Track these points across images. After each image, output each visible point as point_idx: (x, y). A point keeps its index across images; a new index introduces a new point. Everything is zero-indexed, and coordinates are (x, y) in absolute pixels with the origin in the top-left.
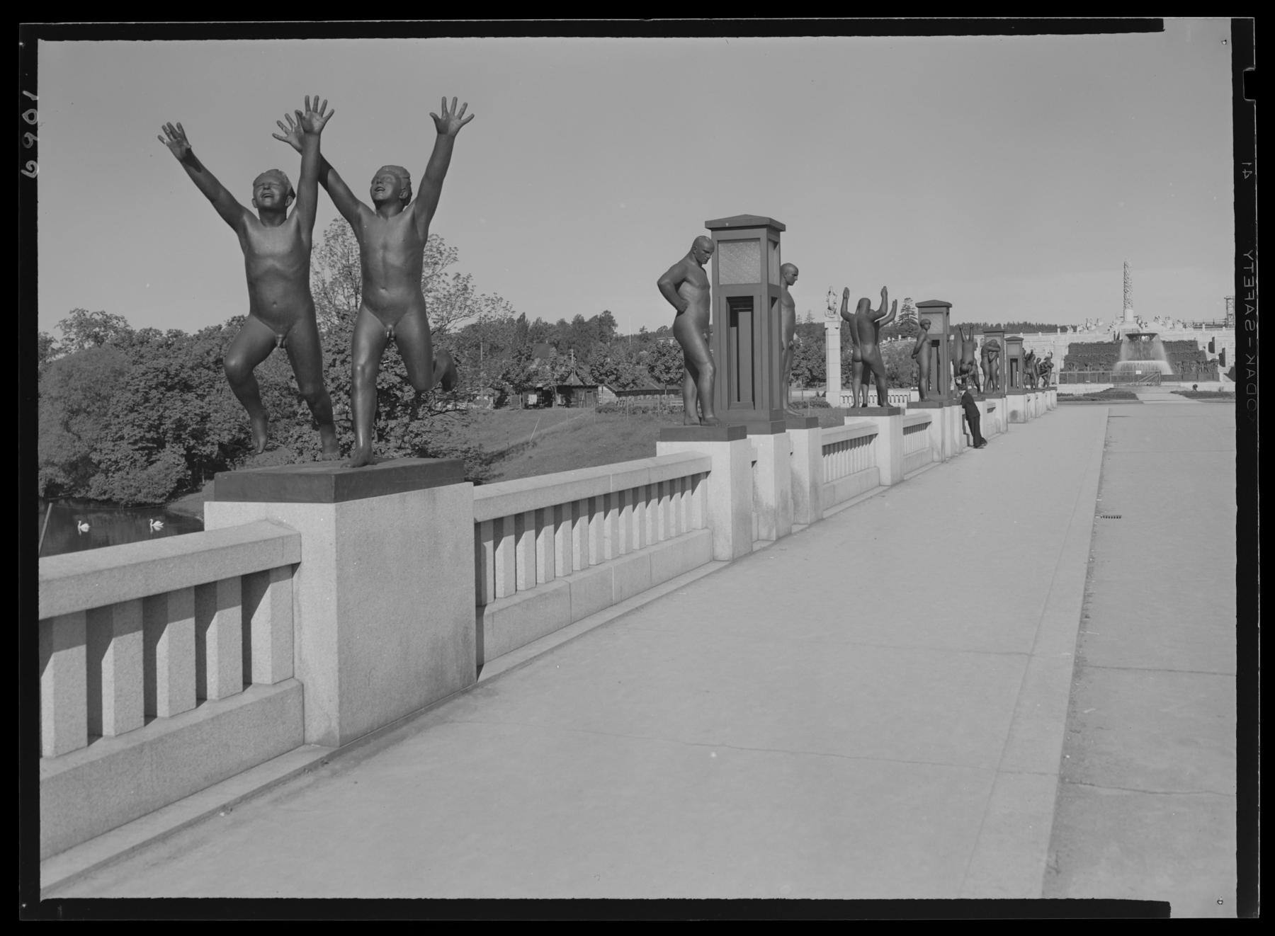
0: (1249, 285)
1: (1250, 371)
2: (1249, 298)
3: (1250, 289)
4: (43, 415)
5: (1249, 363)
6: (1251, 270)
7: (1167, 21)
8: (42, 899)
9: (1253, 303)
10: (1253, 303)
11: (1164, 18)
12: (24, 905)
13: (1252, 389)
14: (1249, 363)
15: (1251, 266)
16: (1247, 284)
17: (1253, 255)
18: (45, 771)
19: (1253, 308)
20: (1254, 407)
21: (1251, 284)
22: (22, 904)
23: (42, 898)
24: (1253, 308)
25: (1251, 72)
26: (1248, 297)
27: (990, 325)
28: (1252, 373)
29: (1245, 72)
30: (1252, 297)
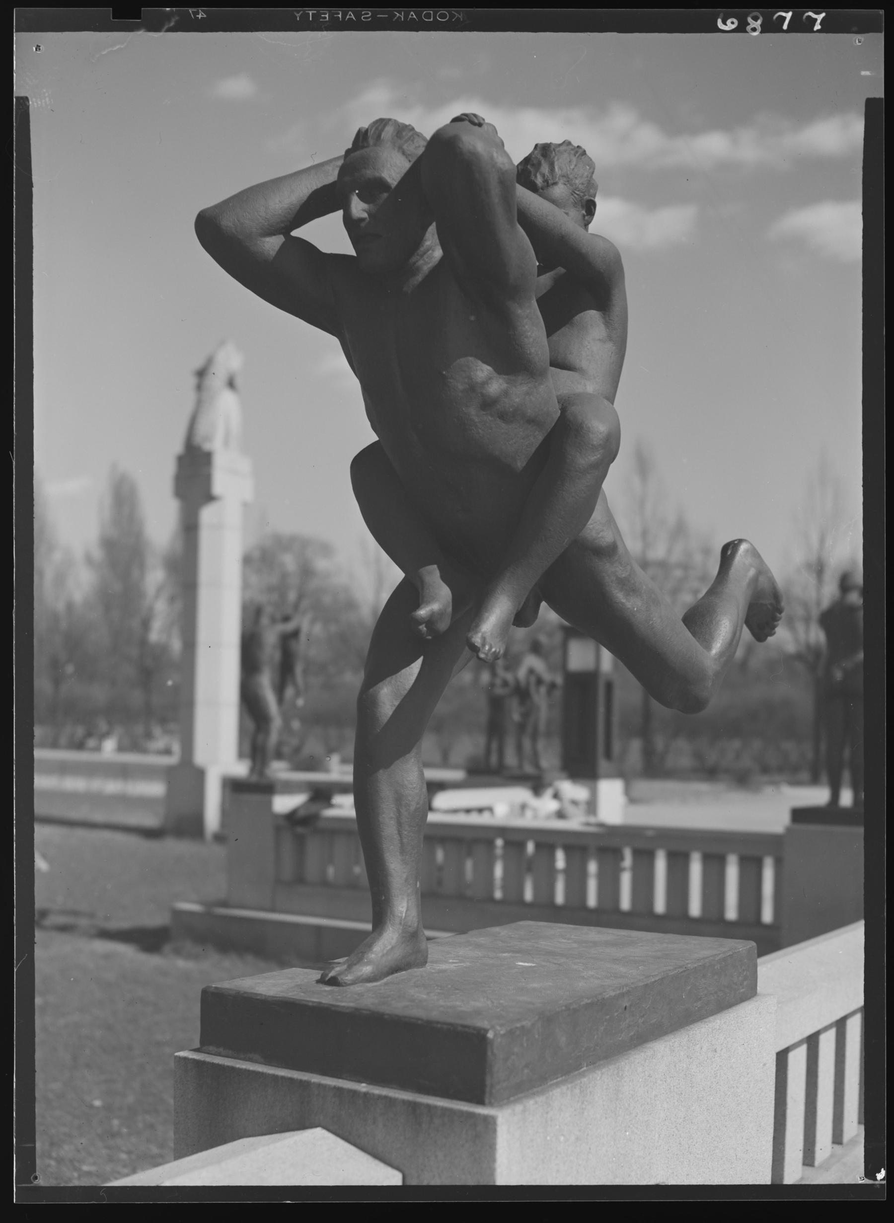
0: (327, 16)
7: (18, 91)
11: (15, 95)
24: (412, 13)
26: (339, 17)
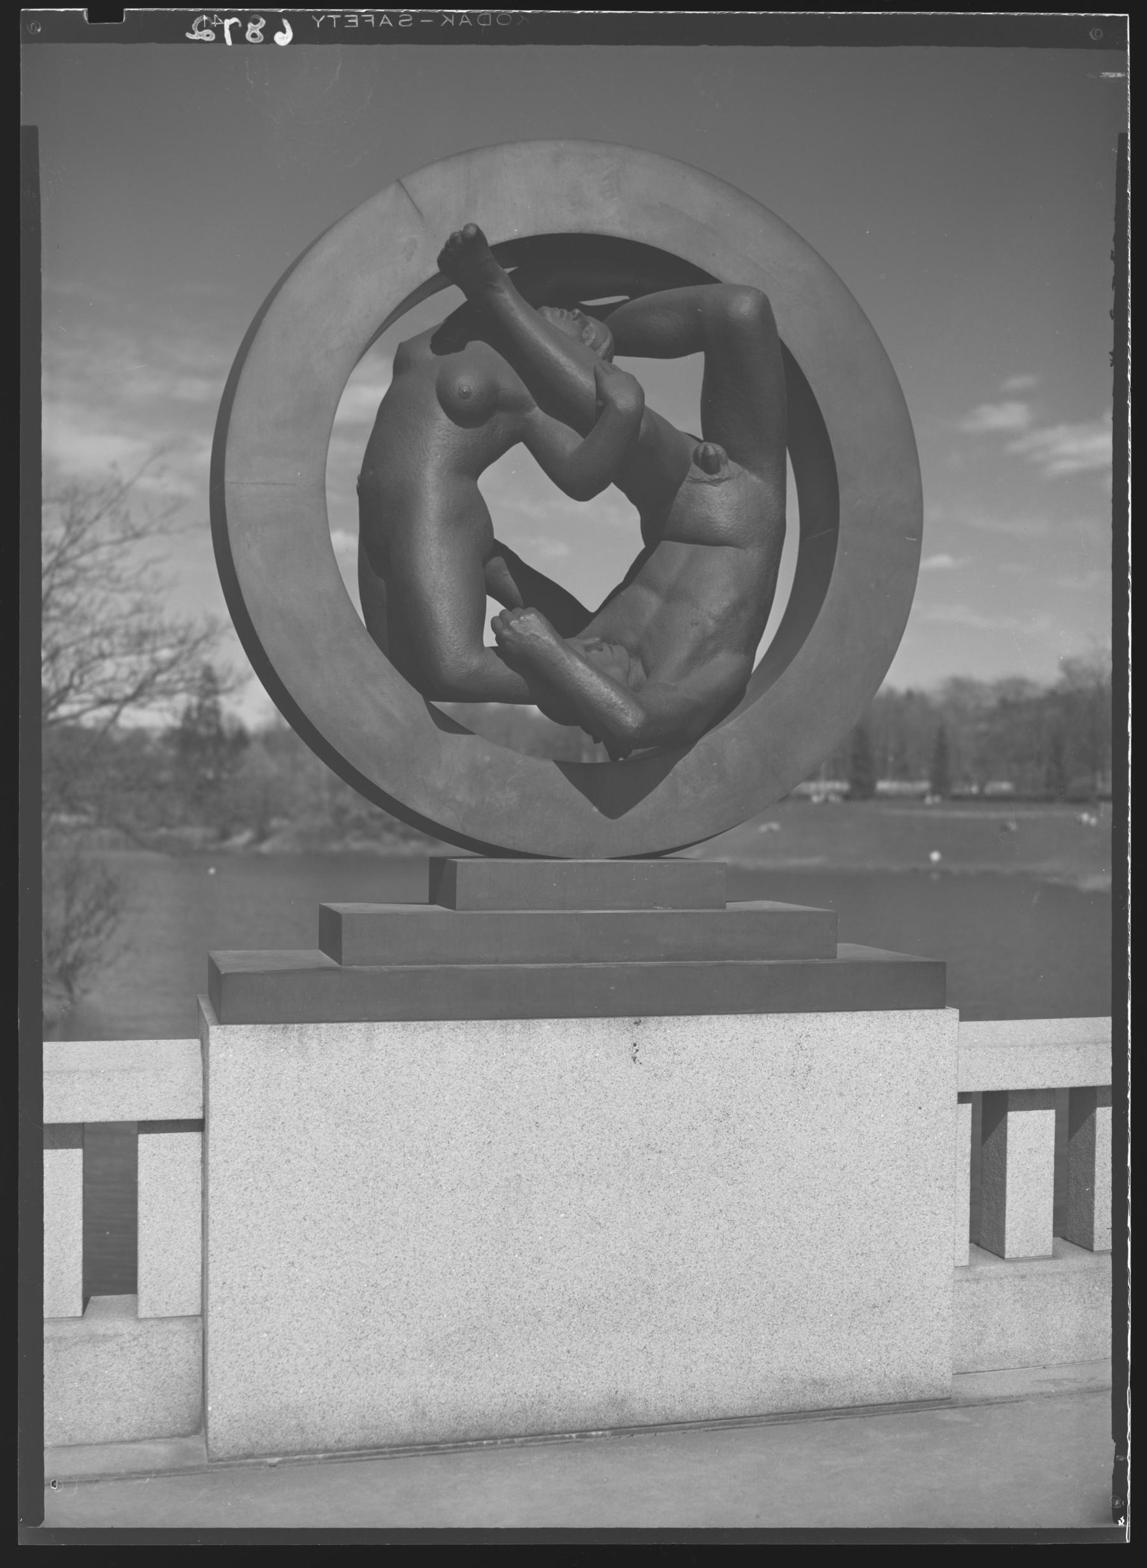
0: (356, 21)
1: (462, 21)
2: (372, 21)
3: (361, 20)
4: (197, 1286)
5: (452, 22)
6: (337, 19)
8: (497, 645)
9: (378, 17)
10: (378, 17)
12: (935, 856)
13: (484, 19)
14: (452, 22)
15: (332, 18)
16: (354, 23)
17: (318, 15)
18: (1106, 1314)
19: (385, 16)
20: (508, 17)
21: (354, 18)
22: (929, 860)
23: (602, 743)
24: (385, 16)
25: (89, 13)
26: (371, 23)
27: (578, 676)
28: (465, 19)
29: (90, 21)
30: (370, 18)
